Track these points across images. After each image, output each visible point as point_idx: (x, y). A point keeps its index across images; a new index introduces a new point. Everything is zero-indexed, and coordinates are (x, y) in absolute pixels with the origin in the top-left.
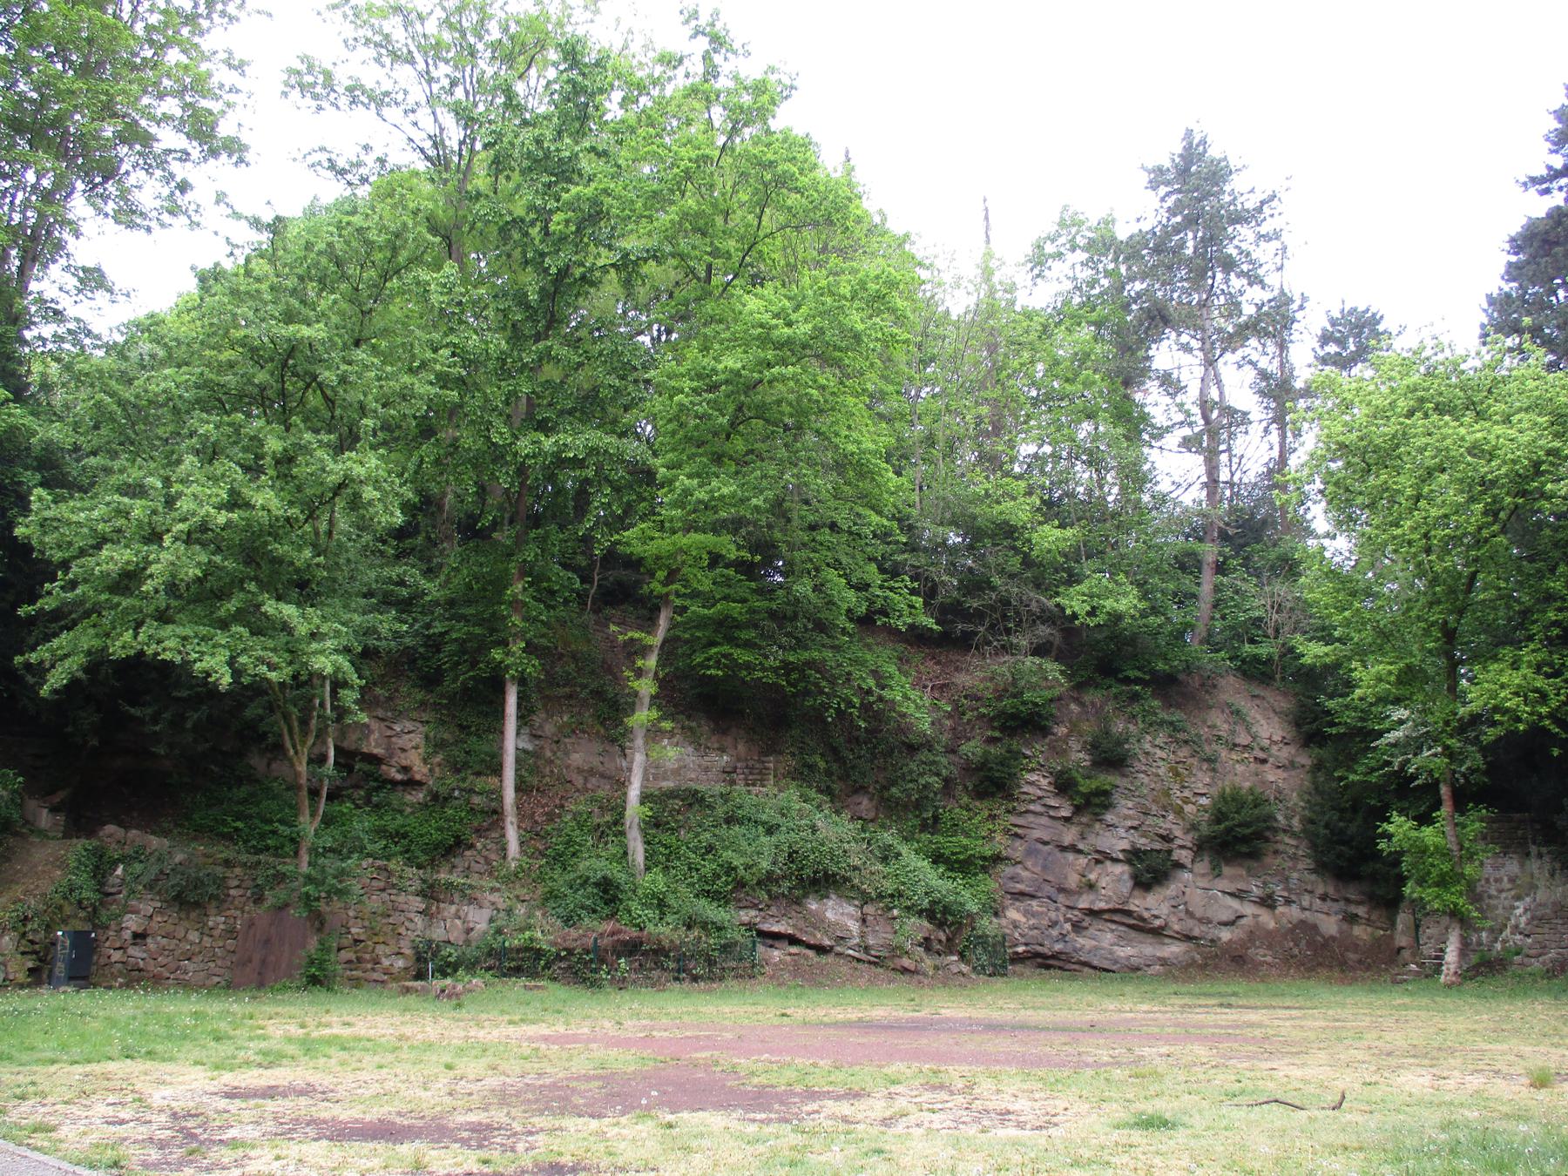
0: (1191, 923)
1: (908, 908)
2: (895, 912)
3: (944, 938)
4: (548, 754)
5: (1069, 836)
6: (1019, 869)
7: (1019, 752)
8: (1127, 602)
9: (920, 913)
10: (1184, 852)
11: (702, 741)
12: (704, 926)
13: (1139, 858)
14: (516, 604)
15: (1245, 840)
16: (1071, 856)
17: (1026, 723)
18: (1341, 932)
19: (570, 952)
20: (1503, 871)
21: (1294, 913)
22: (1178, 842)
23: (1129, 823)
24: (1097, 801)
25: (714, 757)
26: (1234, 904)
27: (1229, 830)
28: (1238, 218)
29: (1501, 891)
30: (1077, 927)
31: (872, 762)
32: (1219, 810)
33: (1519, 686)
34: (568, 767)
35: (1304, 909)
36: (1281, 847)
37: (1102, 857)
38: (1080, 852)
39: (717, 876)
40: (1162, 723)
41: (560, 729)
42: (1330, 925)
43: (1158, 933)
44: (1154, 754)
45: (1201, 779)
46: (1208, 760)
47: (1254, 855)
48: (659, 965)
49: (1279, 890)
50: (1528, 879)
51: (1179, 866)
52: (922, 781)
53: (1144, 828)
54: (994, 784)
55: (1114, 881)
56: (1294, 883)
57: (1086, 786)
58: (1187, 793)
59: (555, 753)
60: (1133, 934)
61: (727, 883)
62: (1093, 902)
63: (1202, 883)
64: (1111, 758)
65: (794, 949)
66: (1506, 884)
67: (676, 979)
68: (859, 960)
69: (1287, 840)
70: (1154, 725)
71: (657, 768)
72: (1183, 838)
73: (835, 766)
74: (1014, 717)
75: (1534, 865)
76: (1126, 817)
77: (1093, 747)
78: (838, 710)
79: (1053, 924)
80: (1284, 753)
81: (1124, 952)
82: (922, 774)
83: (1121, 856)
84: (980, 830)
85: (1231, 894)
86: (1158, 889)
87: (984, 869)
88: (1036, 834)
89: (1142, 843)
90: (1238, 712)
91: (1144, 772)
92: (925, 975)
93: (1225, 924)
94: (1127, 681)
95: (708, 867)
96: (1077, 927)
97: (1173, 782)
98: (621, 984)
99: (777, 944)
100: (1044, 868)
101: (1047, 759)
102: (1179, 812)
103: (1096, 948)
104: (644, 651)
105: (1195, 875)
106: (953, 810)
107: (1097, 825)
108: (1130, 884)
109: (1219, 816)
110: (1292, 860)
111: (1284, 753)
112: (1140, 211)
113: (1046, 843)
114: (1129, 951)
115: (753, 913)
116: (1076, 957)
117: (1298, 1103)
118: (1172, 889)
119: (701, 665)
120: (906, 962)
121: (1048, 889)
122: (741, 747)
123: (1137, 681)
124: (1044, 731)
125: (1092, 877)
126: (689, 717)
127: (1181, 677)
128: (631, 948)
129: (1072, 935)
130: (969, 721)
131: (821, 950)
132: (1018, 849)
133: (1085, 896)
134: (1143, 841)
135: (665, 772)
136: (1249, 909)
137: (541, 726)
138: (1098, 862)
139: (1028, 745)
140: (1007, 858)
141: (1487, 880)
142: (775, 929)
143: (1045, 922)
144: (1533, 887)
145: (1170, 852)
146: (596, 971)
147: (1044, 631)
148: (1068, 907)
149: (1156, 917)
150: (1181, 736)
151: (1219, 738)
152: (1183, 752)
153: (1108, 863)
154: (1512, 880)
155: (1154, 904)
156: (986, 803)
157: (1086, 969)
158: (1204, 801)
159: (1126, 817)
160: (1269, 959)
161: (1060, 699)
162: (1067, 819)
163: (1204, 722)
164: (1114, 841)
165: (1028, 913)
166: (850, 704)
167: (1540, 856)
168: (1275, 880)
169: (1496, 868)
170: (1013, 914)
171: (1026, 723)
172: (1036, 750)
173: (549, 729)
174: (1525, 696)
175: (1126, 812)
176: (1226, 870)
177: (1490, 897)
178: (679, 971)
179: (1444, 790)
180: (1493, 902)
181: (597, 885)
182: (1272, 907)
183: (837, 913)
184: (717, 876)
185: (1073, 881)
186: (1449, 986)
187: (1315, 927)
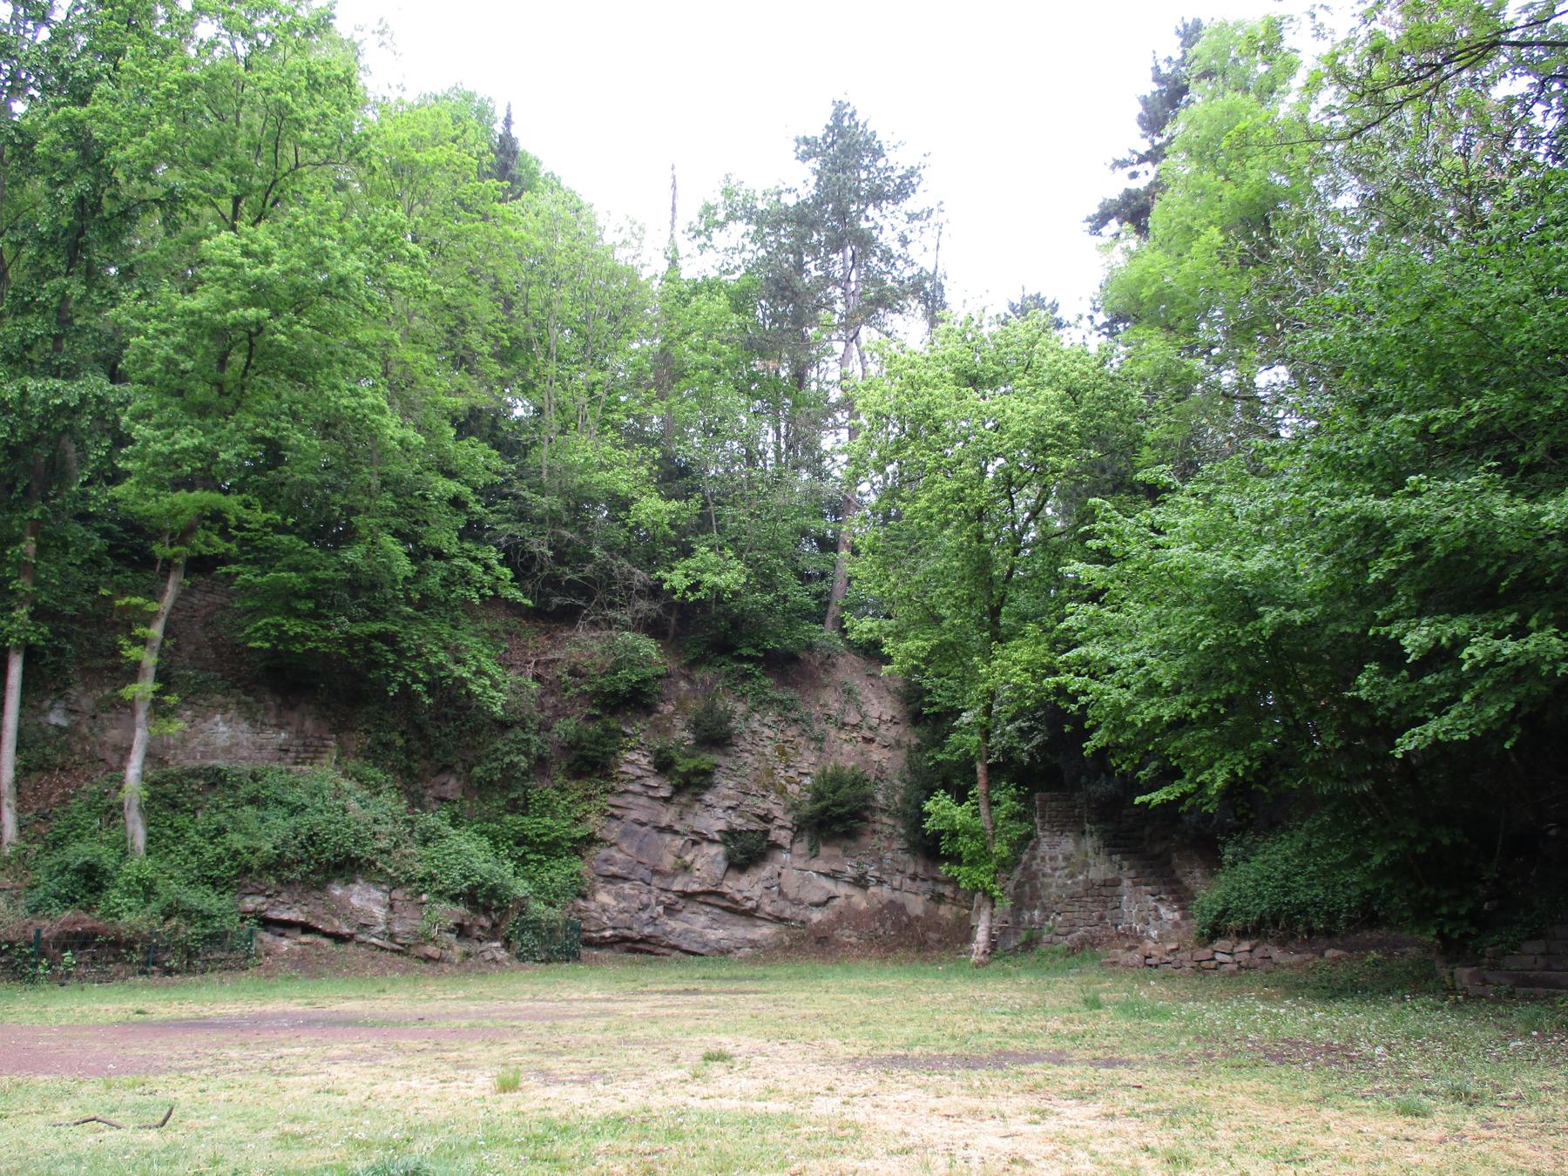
0: (782, 904)
1: (440, 893)
2: (424, 897)
3: (488, 924)
4: (85, 730)
5: (667, 817)
6: (613, 852)
7: (619, 730)
8: (731, 576)
9: (454, 899)
10: (783, 833)
11: (259, 717)
12: (188, 914)
13: (734, 839)
14: (23, 567)
15: (840, 819)
16: (668, 838)
17: (635, 700)
18: (926, 913)
19: (12, 944)
20: (1058, 849)
21: (885, 893)
22: (778, 822)
23: (727, 803)
24: (695, 780)
25: (270, 733)
26: (829, 884)
27: (825, 810)
28: (876, 196)
29: (1055, 869)
30: (670, 910)
31: (459, 739)
32: (817, 790)
33: (1029, 662)
34: (102, 744)
35: (894, 889)
36: (878, 827)
37: (699, 839)
38: (676, 833)
39: (220, 860)
40: (772, 701)
41: (98, 703)
42: (916, 905)
43: (750, 915)
44: (760, 731)
45: (807, 760)
46: (816, 739)
47: (851, 835)
48: (118, 958)
49: (872, 871)
50: (1082, 858)
51: (776, 846)
52: (507, 760)
53: (742, 808)
54: (590, 764)
55: (708, 862)
56: (887, 864)
57: (684, 765)
58: (792, 773)
59: (91, 729)
60: (727, 916)
61: (232, 868)
62: (686, 884)
63: (800, 863)
64: (716, 737)
65: (304, 939)
66: (1061, 863)
67: (143, 972)
68: (383, 949)
69: (885, 819)
70: (763, 703)
71: (206, 745)
72: (783, 817)
73: (416, 744)
74: (615, 694)
75: (1089, 843)
76: (726, 797)
77: (695, 726)
78: (404, 685)
79: (645, 907)
80: (890, 733)
81: (716, 935)
82: (508, 753)
83: (717, 837)
84: (562, 808)
85: (826, 875)
86: (753, 870)
87: (577, 852)
88: (634, 815)
89: (738, 822)
90: (850, 692)
91: (750, 751)
92: (450, 962)
93: (817, 905)
94: (741, 659)
95: (210, 853)
97: (776, 758)
98: (63, 979)
99: (288, 933)
100: (639, 849)
101: (647, 738)
102: (782, 791)
103: (687, 931)
104: (149, 619)
105: (793, 856)
106: (543, 789)
107: (697, 806)
108: (723, 866)
109: (819, 796)
110: (885, 840)
111: (890, 733)
112: (799, 182)
113: (642, 824)
114: (721, 933)
115: (260, 899)
116: (666, 940)
117: (165, 1112)
118: (767, 871)
119: (249, 637)
120: (431, 950)
121: (641, 871)
122: (309, 725)
123: (750, 659)
124: (649, 709)
125: (688, 858)
126: (247, 693)
127: (803, 655)
128: (80, 941)
129: (664, 919)
130: (570, 698)
131: (339, 938)
132: (614, 831)
134: (740, 821)
135: (215, 750)
136: (842, 890)
137: (77, 701)
138: (695, 843)
139: (629, 723)
140: (602, 840)
141: (1043, 859)
142: (285, 916)
143: (636, 905)
144: (1085, 865)
145: (766, 833)
146: (35, 965)
147: (643, 605)
148: (663, 890)
149: (748, 899)
150: (794, 715)
151: (829, 717)
152: (792, 732)
153: (705, 844)
154: (1066, 858)
155: (747, 886)
156: (583, 783)
157: (676, 954)
158: (807, 781)
159: (726, 797)
160: (853, 940)
161: (669, 676)
162: (666, 800)
163: (818, 700)
164: (712, 821)
165: (619, 896)
166: (416, 680)
167: (1091, 834)
168: (868, 860)
169: (1052, 846)
170: (604, 897)
171: (635, 700)
172: (636, 728)
173: (86, 703)
174: (1034, 673)
175: (726, 791)
176: (824, 850)
177: (1044, 875)
178: (147, 964)
179: (980, 768)
180: (1046, 880)
181: (77, 871)
182: (865, 887)
183: (364, 899)
184: (220, 860)
185: (668, 862)
186: (978, 965)
187: (902, 907)
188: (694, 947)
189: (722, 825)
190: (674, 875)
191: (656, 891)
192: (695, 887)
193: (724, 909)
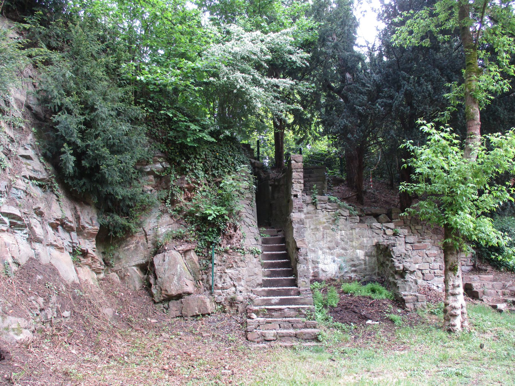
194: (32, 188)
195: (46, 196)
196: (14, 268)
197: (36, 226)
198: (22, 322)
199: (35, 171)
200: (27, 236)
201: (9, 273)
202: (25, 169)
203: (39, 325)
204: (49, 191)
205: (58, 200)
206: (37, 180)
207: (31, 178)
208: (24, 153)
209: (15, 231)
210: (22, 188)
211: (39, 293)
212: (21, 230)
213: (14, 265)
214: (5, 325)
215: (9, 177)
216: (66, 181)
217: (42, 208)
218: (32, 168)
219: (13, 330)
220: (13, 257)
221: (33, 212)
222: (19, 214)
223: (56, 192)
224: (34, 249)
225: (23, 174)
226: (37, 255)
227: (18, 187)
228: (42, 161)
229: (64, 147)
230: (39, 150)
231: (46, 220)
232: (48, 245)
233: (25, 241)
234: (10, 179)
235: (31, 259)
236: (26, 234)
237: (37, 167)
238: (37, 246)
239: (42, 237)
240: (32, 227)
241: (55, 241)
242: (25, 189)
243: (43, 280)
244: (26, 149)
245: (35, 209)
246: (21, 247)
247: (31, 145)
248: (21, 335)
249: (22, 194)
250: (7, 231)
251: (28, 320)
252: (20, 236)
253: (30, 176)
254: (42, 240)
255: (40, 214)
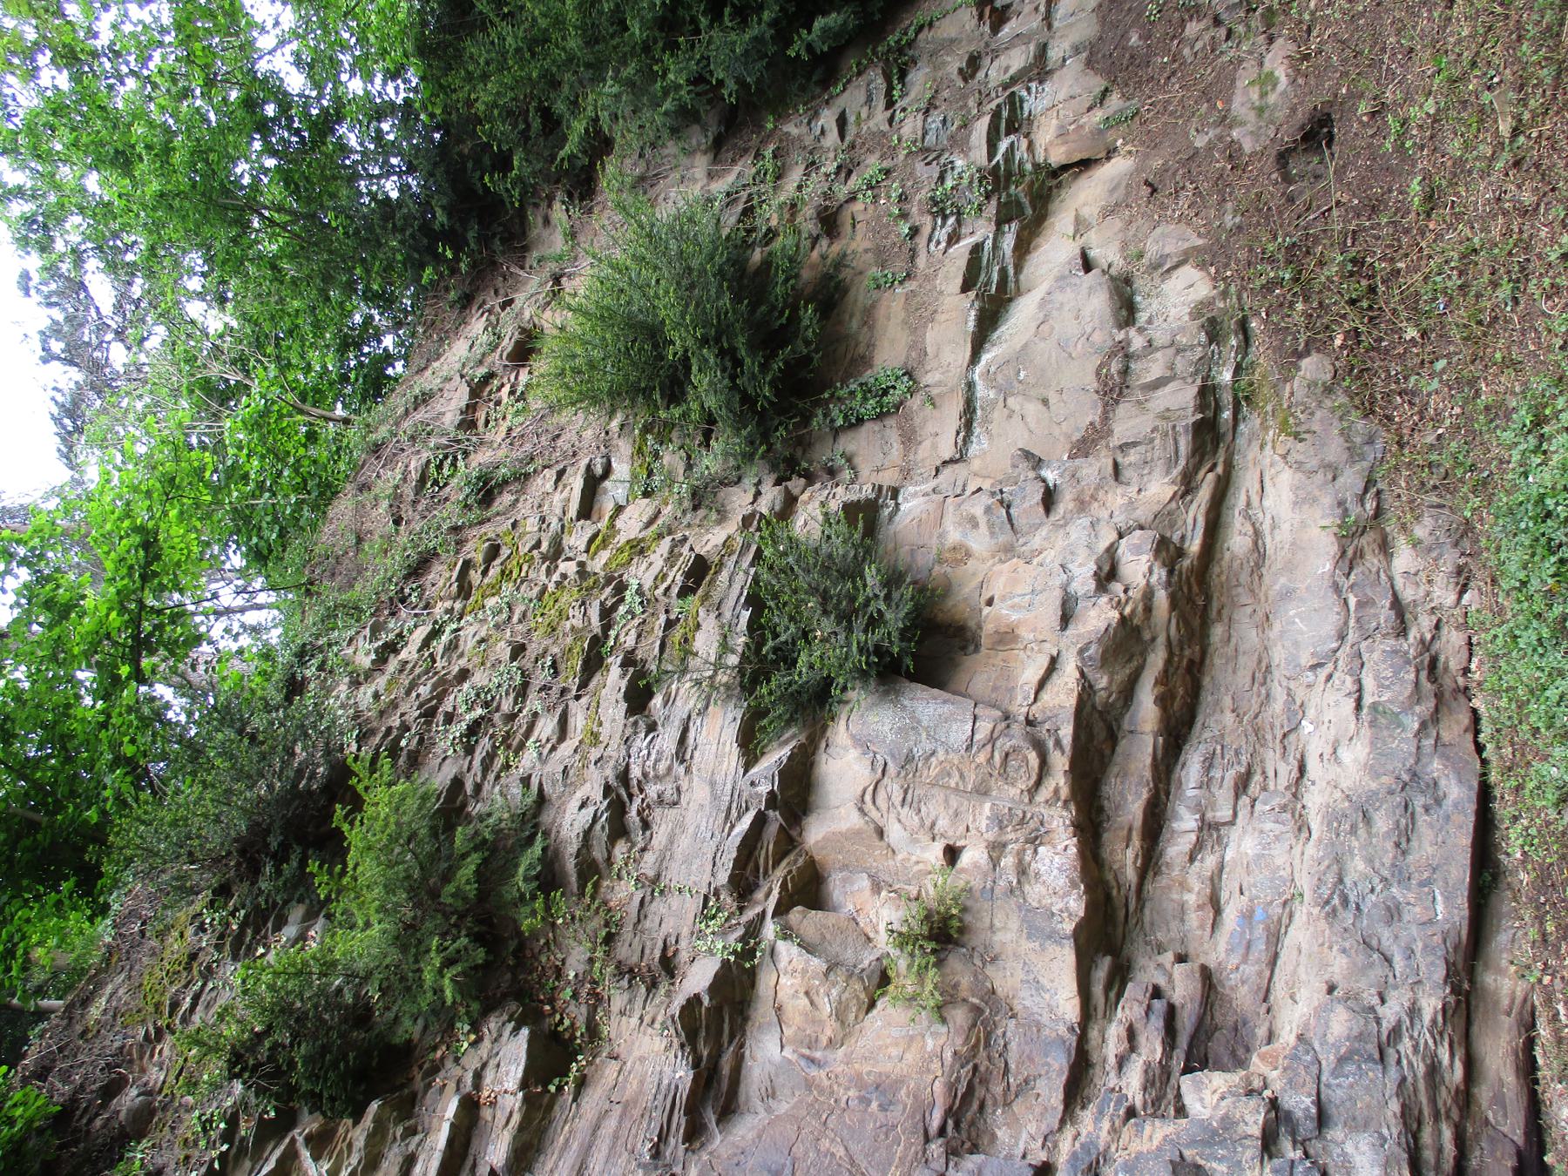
5: (644, 1054)
16: (766, 1052)
30: (1204, 1036)
37: (778, 860)
43: (1199, 589)
47: (831, 293)
55: (913, 800)
60: (1218, 722)
62: (1037, 925)
83: (775, 757)
96: (1204, 1036)
103: (1337, 901)
108: (925, 704)
133: (1006, 980)
138: (809, 890)
149: (1107, 575)
153: (816, 833)
155: (1040, 600)
164: (697, 793)
176: (888, 355)
185: (905, 1046)
188: (1446, 844)
189: (718, 733)
190: (985, 1018)
191: (1092, 1124)
192: (1057, 860)
193: (1177, 731)
194: (912, 95)
195: (925, 57)
196: (1115, 101)
197: (1007, 69)
198: (1245, 76)
199: (869, 100)
200: (1033, 85)
201: (1129, 113)
202: (871, 124)
203: (1256, 21)
204: (911, 53)
205: (931, 25)
206: (890, 89)
207: (890, 104)
208: (832, 137)
209: (1026, 114)
210: (919, 123)
211: (1174, 37)
212: (1022, 101)
213: (1107, 102)
214: (1251, 116)
215: (901, 157)
216: (877, 17)
217: (958, 65)
218: (865, 109)
219: (1263, 95)
220: (1090, 109)
221: (973, 83)
222: (986, 120)
223: (911, 33)
224: (1064, 60)
225: (885, 127)
226: (1077, 50)
227: (920, 133)
228: (840, 87)
229: (798, 55)
230: (813, 98)
231: (987, 45)
232: (1050, 26)
233: (1048, 86)
234: (907, 155)
235: (1089, 64)
236: (1028, 89)
237: (859, 97)
238: (1054, 54)
239: (1032, 47)
240: (1012, 78)
241: (1036, 9)
242: (920, 116)
243: (1143, 27)
244: (823, 132)
245: (965, 80)
246: (1061, 96)
247: (809, 123)
248: (1277, 73)
249: (935, 119)
250: (1027, 135)
251: (1241, 61)
252: (1036, 101)
253: (887, 108)
254: (1038, 45)
255: (974, 62)
